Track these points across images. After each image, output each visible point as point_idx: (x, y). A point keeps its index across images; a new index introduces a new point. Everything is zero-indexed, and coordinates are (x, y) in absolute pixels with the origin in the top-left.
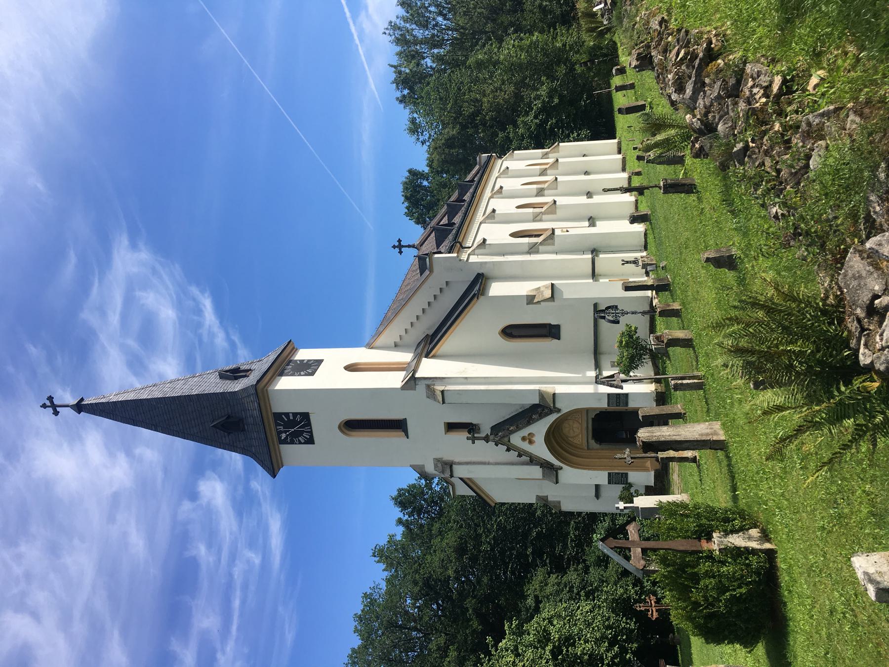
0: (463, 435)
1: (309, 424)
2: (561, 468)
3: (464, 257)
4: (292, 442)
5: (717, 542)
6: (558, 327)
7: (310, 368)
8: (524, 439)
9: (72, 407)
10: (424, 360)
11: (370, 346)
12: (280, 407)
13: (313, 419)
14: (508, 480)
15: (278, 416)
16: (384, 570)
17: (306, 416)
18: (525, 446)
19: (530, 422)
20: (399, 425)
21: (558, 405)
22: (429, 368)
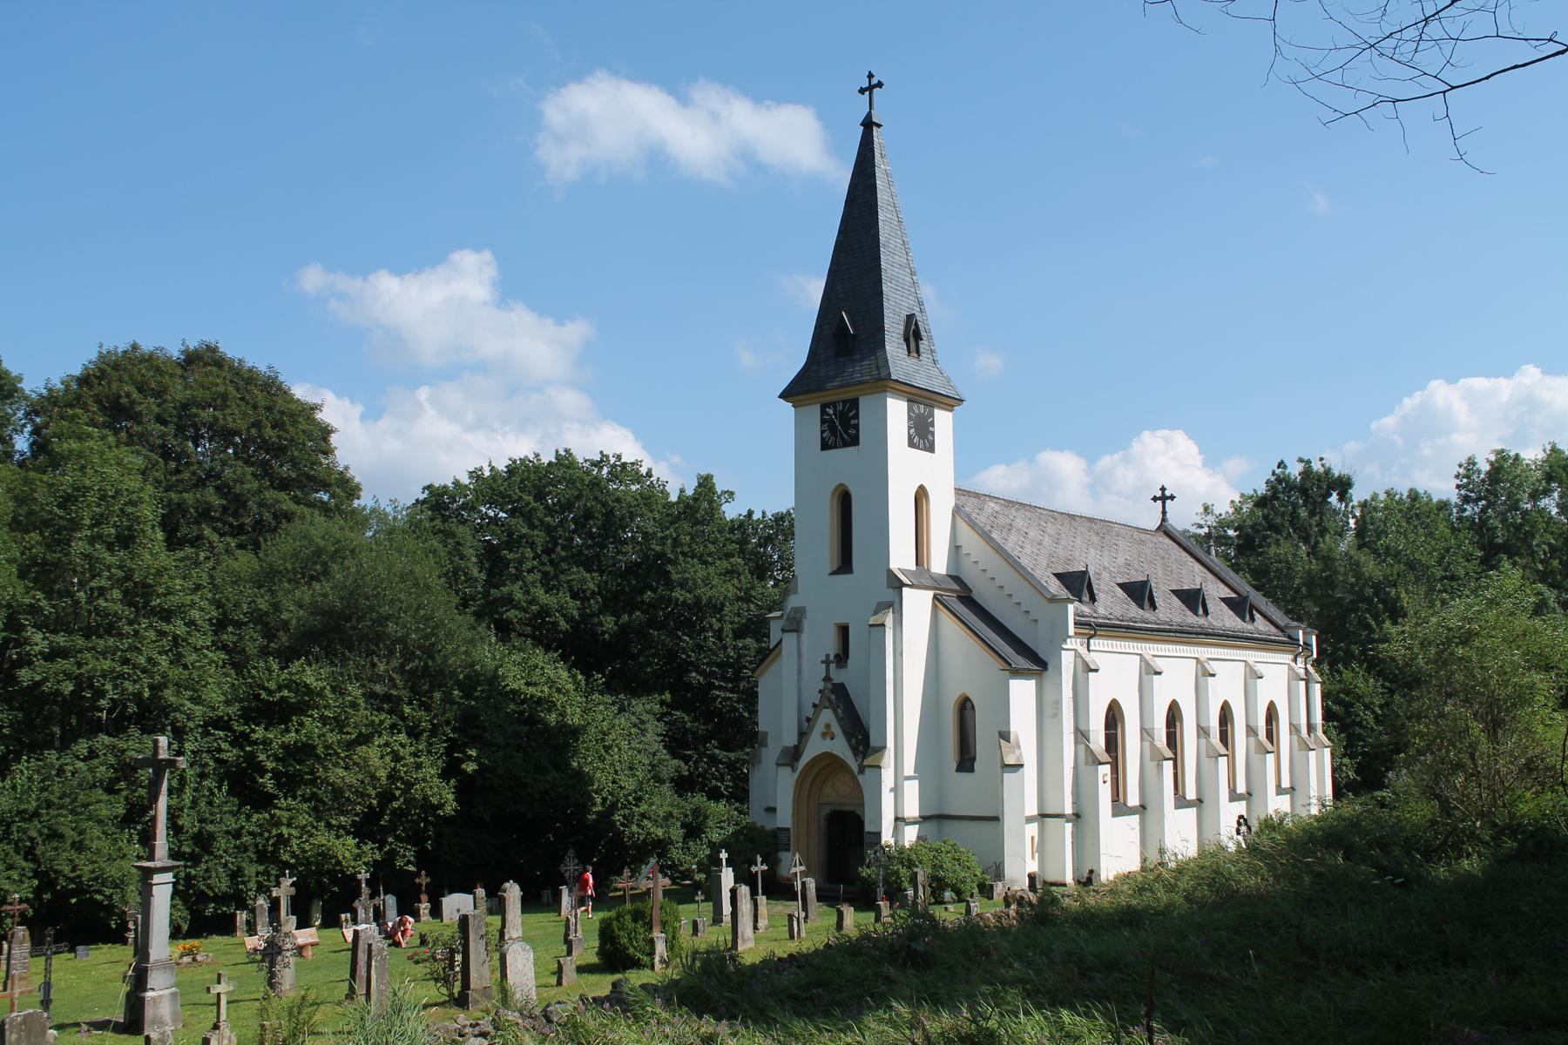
0: (831, 647)
1: (846, 444)
2: (794, 770)
3: (1073, 643)
4: (823, 422)
5: (657, 934)
6: (971, 770)
7: (922, 436)
8: (828, 726)
9: (869, 115)
10: (931, 594)
11: (957, 511)
12: (865, 405)
13: (851, 450)
14: (785, 694)
15: (854, 404)
16: (682, 491)
17: (854, 441)
18: (819, 727)
19: (848, 736)
20: (845, 564)
21: (867, 771)
22: (917, 605)
